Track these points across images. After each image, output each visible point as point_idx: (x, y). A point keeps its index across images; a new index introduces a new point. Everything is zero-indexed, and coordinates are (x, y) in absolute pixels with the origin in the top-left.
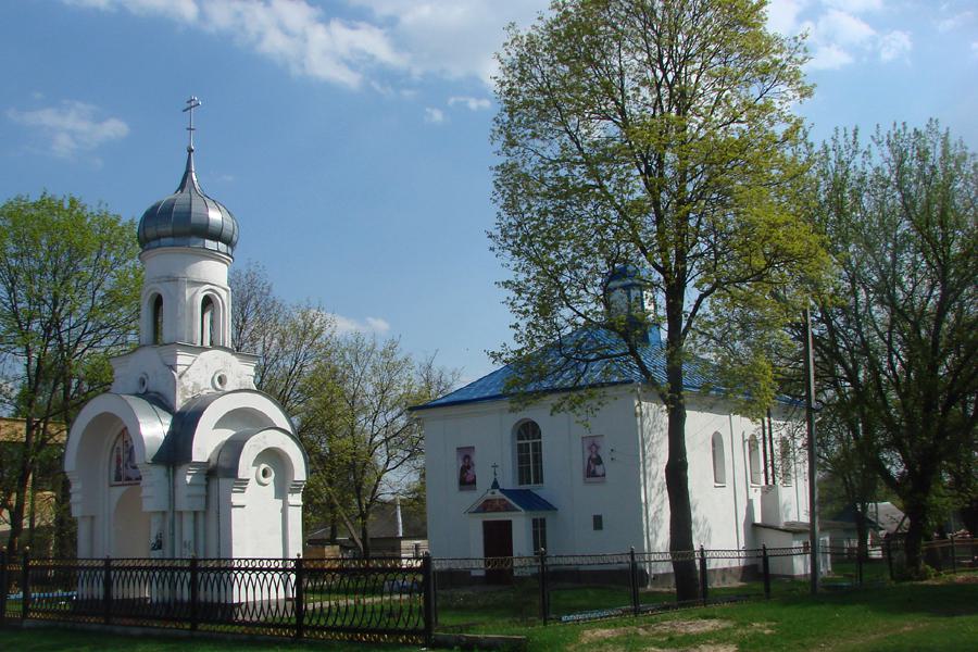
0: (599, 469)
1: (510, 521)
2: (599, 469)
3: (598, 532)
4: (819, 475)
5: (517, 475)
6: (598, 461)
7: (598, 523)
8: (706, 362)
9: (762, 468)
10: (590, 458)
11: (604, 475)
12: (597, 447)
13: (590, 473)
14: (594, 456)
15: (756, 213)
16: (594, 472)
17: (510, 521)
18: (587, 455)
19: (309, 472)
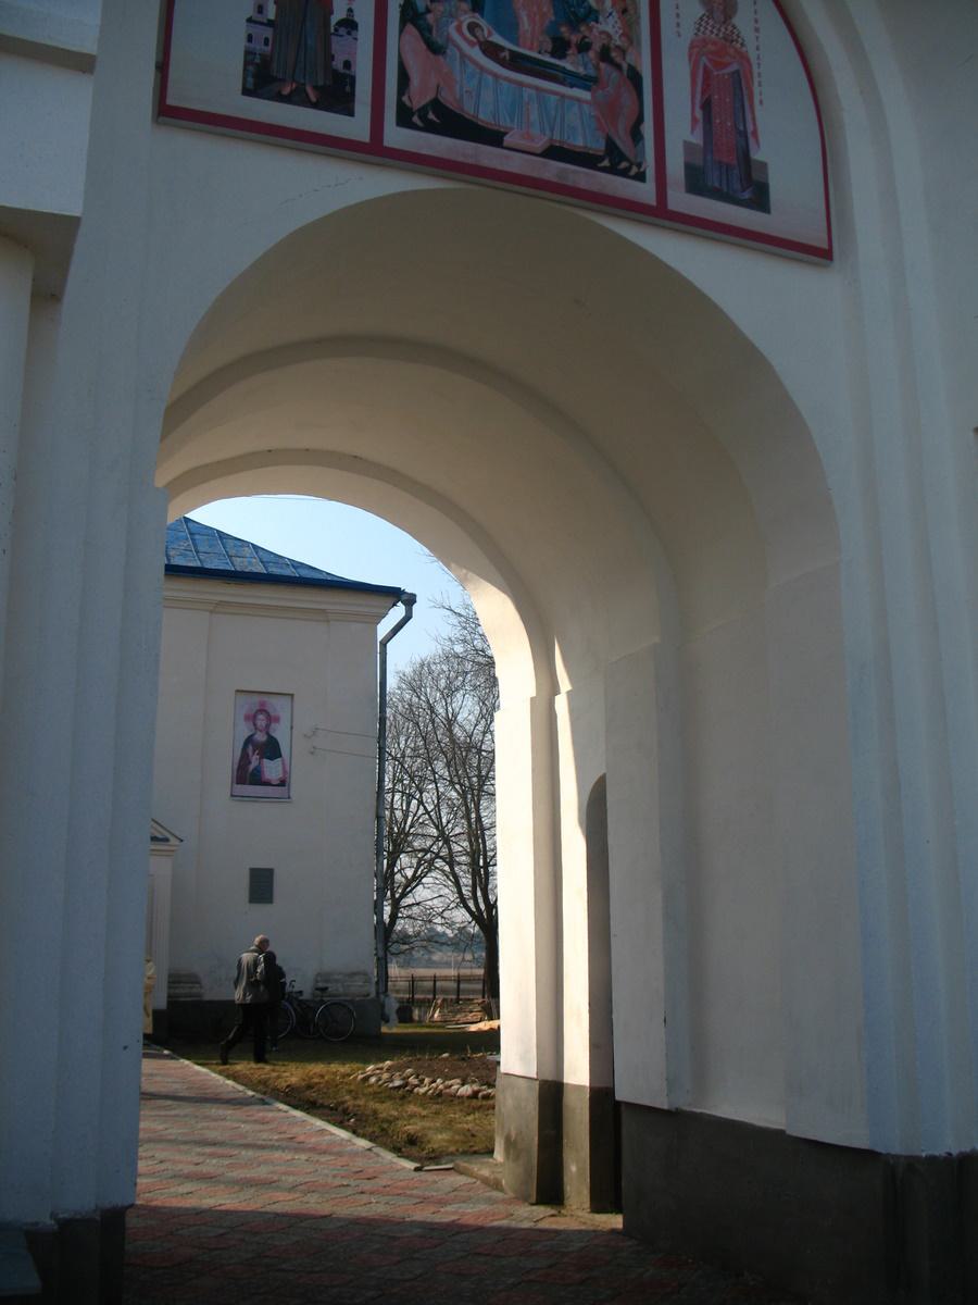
0: (272, 769)
1: (246, 92)
2: (272, 769)
3: (261, 909)
4: (348, 89)
5: (178, 576)
6: (271, 749)
7: (261, 886)
8: (448, 765)
9: (557, 206)
10: (249, 741)
11: (282, 783)
12: (272, 719)
13: (246, 775)
14: (261, 737)
15: (459, 920)
16: (258, 771)
17: (246, 92)
18: (244, 731)
19: (277, 14)
